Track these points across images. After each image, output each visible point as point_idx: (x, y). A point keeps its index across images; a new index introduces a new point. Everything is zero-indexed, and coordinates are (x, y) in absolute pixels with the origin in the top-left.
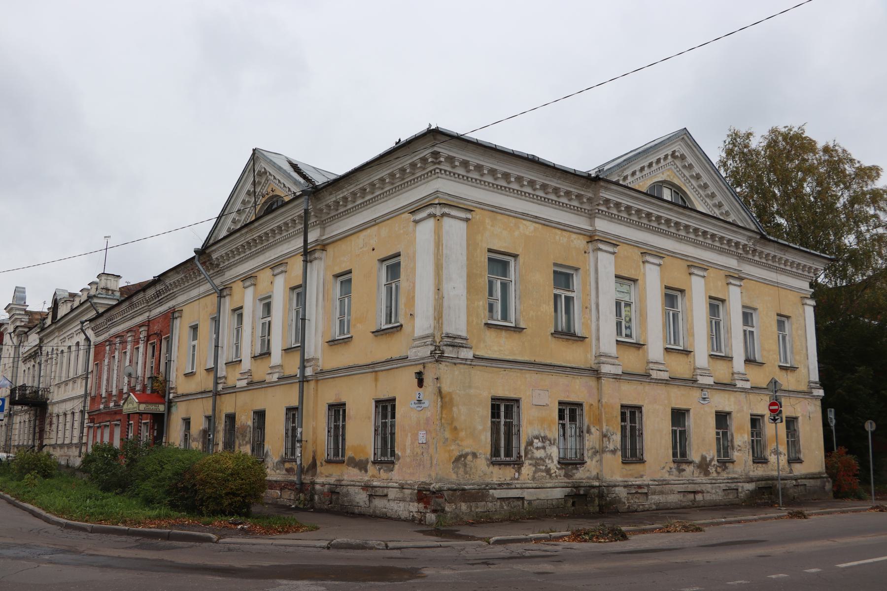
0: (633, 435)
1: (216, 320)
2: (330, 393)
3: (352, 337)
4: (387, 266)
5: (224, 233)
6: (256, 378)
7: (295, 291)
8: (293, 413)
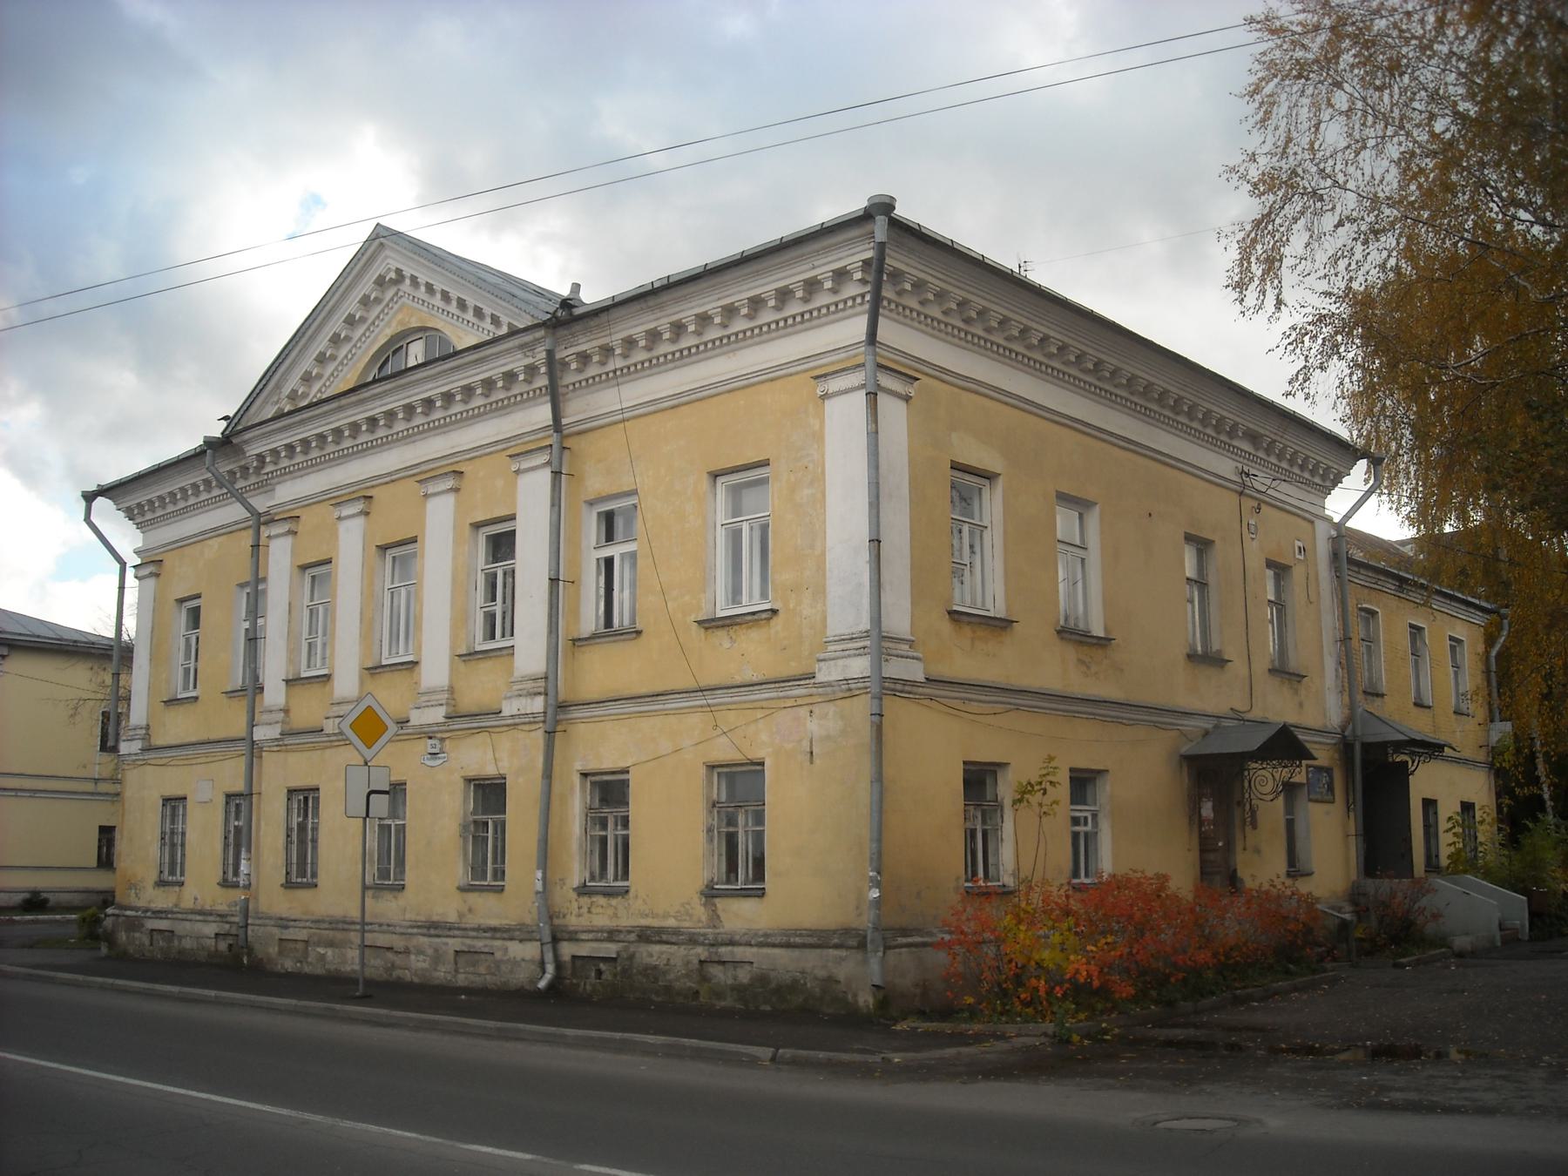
0: (302, 842)
1: (255, 588)
2: (295, 768)
3: (196, 698)
4: (599, 513)
5: (270, 412)
6: (468, 702)
7: (308, 571)
8: (239, 803)
